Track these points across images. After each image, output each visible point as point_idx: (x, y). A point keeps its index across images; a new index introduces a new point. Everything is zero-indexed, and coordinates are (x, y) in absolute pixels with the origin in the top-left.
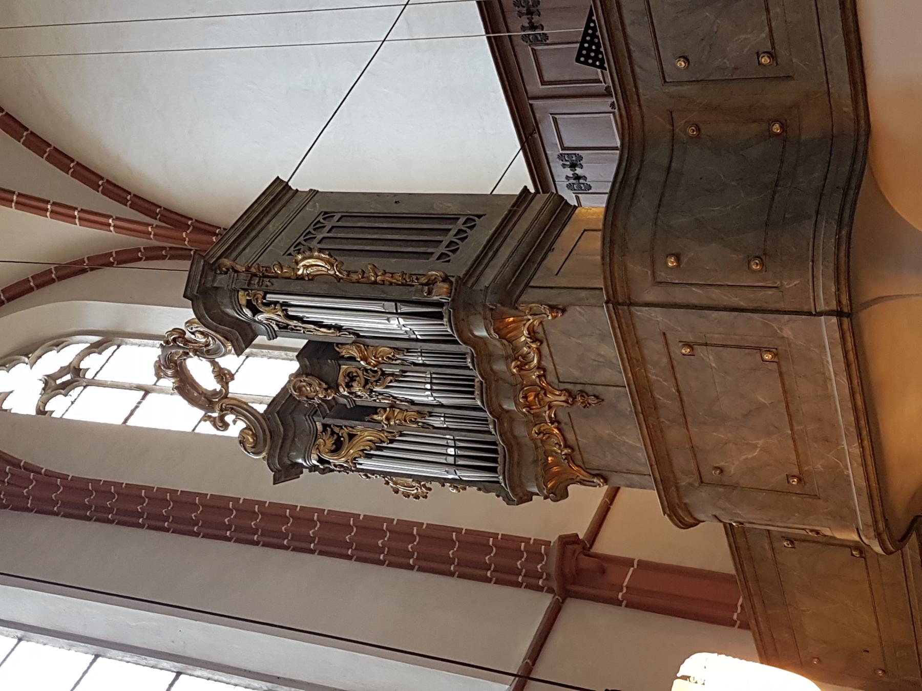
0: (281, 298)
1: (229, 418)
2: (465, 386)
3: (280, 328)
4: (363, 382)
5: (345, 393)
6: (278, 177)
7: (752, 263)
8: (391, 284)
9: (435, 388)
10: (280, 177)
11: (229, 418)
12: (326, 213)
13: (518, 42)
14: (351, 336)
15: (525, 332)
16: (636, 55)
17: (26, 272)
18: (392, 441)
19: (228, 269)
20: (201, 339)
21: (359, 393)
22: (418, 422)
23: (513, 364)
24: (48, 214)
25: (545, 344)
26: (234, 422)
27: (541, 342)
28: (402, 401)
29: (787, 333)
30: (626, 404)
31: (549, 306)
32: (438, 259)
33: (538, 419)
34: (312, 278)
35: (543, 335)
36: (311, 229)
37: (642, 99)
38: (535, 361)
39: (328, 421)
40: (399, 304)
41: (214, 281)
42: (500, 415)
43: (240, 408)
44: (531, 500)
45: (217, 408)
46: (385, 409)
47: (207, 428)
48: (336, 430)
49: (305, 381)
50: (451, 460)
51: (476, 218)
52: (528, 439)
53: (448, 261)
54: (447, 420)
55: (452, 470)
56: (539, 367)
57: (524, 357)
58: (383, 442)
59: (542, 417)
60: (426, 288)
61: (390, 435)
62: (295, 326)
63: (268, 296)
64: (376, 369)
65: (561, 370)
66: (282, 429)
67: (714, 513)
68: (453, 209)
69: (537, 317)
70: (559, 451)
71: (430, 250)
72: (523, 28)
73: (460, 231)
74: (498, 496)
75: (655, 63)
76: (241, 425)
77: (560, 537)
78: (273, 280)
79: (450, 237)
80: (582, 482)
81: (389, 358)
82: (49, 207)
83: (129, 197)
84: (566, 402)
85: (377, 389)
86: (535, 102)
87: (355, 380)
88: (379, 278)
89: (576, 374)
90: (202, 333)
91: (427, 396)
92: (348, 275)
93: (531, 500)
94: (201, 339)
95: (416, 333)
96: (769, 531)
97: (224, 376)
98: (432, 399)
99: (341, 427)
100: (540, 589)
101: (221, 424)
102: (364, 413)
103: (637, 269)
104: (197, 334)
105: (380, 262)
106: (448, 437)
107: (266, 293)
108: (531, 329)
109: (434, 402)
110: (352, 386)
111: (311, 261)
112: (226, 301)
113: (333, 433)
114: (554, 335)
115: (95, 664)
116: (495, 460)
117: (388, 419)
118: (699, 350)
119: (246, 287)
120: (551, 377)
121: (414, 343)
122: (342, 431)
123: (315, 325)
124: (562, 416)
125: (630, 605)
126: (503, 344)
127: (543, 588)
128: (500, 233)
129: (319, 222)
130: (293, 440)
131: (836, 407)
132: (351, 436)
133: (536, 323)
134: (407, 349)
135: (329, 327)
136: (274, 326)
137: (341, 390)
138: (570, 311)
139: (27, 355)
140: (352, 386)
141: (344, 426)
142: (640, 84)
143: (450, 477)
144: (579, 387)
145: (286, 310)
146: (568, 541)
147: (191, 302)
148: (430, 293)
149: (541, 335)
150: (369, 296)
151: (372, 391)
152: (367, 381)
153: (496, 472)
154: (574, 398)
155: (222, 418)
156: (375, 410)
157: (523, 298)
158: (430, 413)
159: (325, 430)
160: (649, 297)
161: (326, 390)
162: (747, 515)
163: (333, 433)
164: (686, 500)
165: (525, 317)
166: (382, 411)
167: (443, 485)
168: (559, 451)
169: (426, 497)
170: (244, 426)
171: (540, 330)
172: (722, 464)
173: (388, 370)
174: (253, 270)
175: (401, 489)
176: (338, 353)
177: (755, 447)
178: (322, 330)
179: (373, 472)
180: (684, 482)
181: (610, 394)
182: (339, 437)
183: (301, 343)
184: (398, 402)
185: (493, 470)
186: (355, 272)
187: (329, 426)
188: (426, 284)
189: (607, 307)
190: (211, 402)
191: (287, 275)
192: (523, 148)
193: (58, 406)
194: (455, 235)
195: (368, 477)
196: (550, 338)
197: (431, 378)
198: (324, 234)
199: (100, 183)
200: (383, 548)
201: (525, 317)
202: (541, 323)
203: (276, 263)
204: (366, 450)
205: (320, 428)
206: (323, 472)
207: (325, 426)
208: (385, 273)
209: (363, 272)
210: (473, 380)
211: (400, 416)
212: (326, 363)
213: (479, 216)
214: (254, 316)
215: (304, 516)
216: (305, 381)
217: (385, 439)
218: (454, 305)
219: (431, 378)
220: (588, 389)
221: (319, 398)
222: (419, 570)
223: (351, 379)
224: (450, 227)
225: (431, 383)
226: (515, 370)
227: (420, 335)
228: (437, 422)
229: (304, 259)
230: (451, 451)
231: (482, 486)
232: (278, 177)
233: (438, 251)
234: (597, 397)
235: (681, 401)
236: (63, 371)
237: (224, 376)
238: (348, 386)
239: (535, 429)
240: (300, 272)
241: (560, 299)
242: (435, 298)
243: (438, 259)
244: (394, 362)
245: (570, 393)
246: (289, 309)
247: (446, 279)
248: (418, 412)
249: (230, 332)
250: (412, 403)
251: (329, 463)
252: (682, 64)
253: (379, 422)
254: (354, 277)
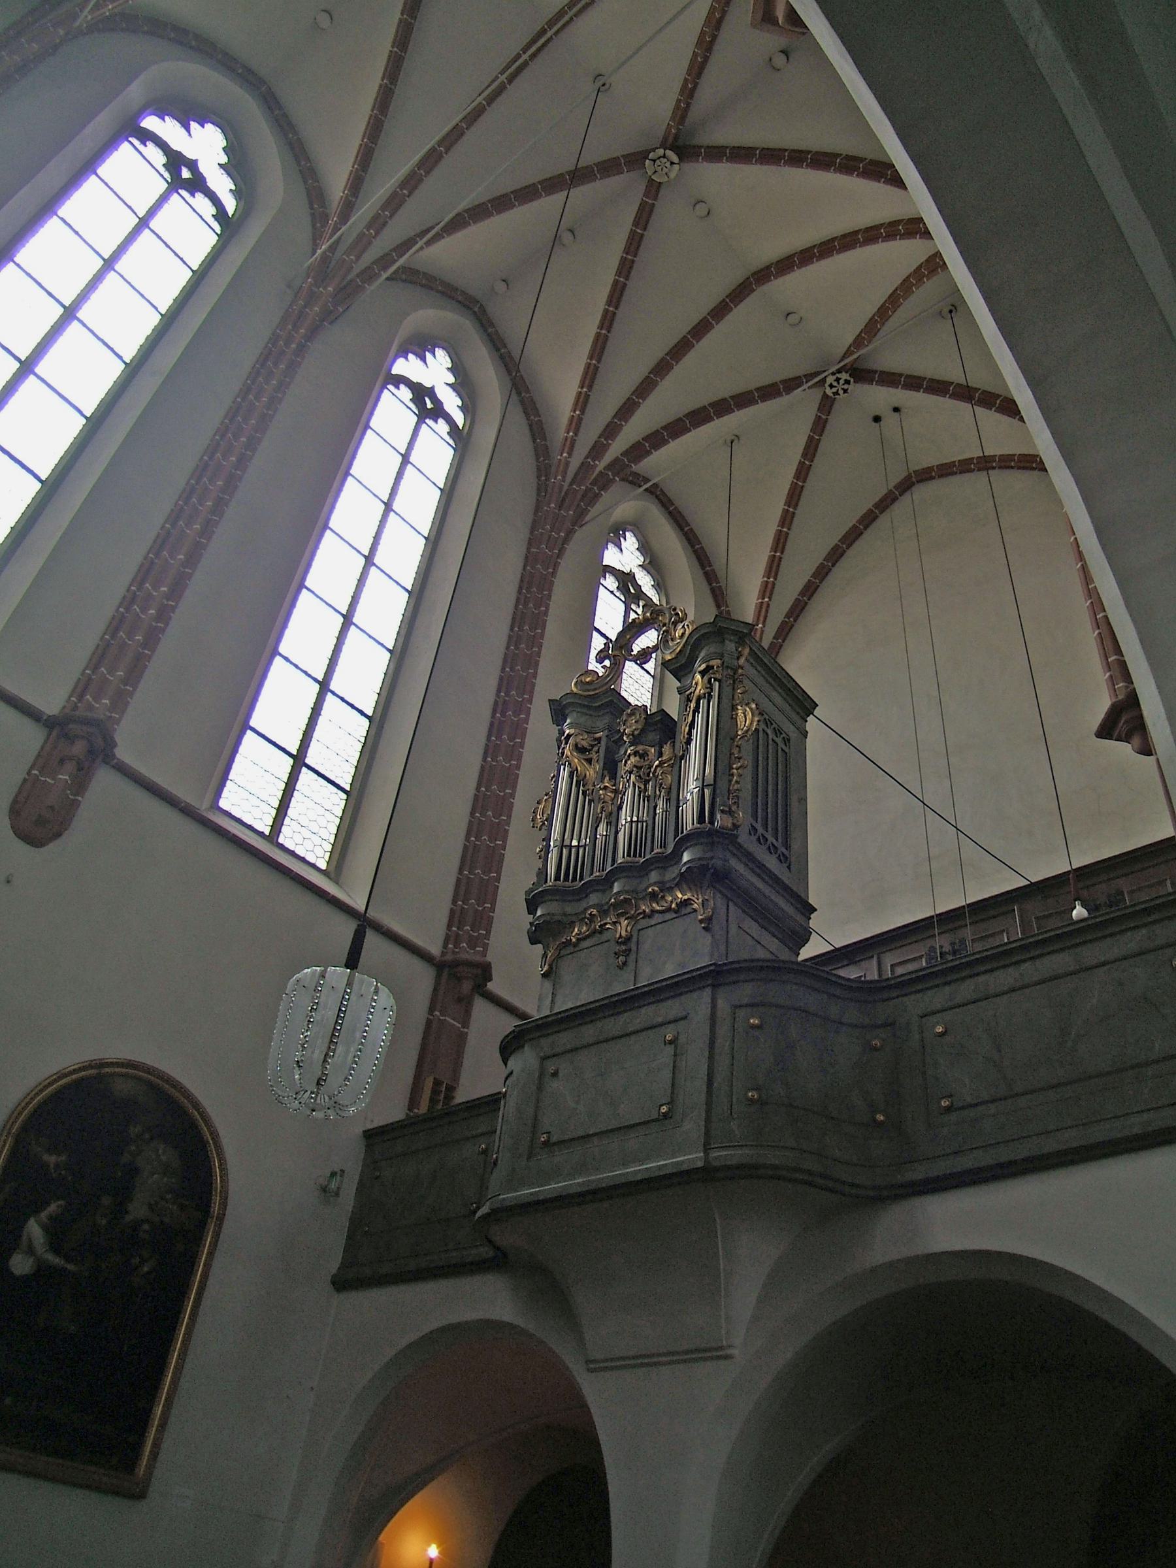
0: (715, 694)
1: (607, 663)
2: (634, 849)
3: (688, 696)
4: (639, 765)
5: (629, 751)
6: (817, 705)
7: (755, 1093)
8: (730, 781)
9: (634, 824)
10: (817, 708)
11: (607, 663)
12: (789, 740)
13: (929, 943)
14: (681, 753)
15: (686, 897)
16: (947, 989)
17: (718, 564)
18: (584, 793)
19: (740, 652)
20: (678, 633)
21: (629, 762)
22: (602, 813)
23: (656, 889)
24: (766, 579)
25: (675, 916)
26: (603, 667)
27: (676, 912)
28: (621, 798)
29: (687, 1126)
30: (618, 988)
31: (712, 916)
32: (752, 826)
33: (604, 913)
34: (734, 719)
35: (683, 913)
36: (775, 725)
37: (905, 999)
38: (658, 908)
39: (603, 742)
40: (712, 787)
41: (731, 641)
42: (606, 882)
43: (616, 671)
44: (529, 914)
45: (616, 653)
46: (614, 785)
47: (598, 643)
48: (596, 749)
49: (640, 717)
50: (567, 842)
51: (787, 864)
52: (585, 906)
53: (750, 834)
54: (604, 837)
55: (558, 843)
56: (653, 911)
57: (663, 897)
58: (584, 786)
59: (607, 918)
60: (727, 809)
61: (591, 791)
62: (690, 707)
63: (717, 683)
64: (651, 775)
65: (650, 931)
66: (597, 704)
67: (514, 1073)
68: (795, 846)
69: (701, 907)
70: (574, 934)
71: (759, 819)
72: (941, 947)
73: (776, 848)
74: (533, 884)
75: (939, 1006)
76: (601, 672)
77: (490, 963)
78: (731, 687)
79: (771, 839)
80: (545, 955)
81: (661, 784)
82: (778, 554)
83: (791, 619)
84: (621, 936)
85: (633, 777)
86: (874, 961)
87: (640, 758)
88: (735, 771)
89: (646, 946)
90: (683, 634)
91: (626, 819)
92: (737, 746)
93: (529, 914)
94: (678, 633)
95: (685, 806)
96: (496, 1132)
97: (643, 657)
98: (624, 823)
99: (598, 752)
100: (445, 946)
101: (602, 656)
102: (611, 767)
103: (746, 992)
104: (682, 631)
105: (748, 773)
106: (588, 840)
107: (719, 681)
108: (688, 902)
109: (620, 826)
110: (635, 756)
111: (749, 716)
112: (712, 650)
113: (593, 746)
114: (680, 924)
115: (385, 650)
116: (566, 878)
117: (605, 788)
118: (670, 1049)
119: (725, 664)
120: (644, 923)
121: (675, 805)
122: (594, 753)
123: (691, 721)
124: (606, 936)
125: (429, 1023)
126: (674, 879)
127: (432, 1015)
128: (776, 881)
129: (781, 733)
130: (587, 714)
131: (616, 1171)
132: (589, 761)
133: (695, 906)
134: (669, 799)
135: (690, 733)
136: (690, 691)
137: (632, 748)
138: (708, 937)
139: (650, 563)
140: (635, 756)
141: (598, 757)
142: (919, 996)
143: (552, 843)
144: (634, 948)
145: (705, 697)
146: (485, 972)
147: (712, 621)
148: (722, 811)
149: (684, 911)
150: (719, 762)
151: (631, 773)
152: (639, 768)
153: (555, 880)
154: (624, 943)
155: (608, 657)
156: (613, 777)
157: (718, 895)
158: (611, 823)
159: (595, 739)
160: (721, 1003)
161: (633, 735)
162: (509, 1108)
163: (593, 746)
164: (526, 1048)
165: (700, 896)
166: (612, 783)
167: (543, 840)
168: (574, 934)
169: (533, 827)
170: (600, 674)
171: (689, 910)
172: (561, 1074)
173: (650, 786)
174: (740, 671)
175: (541, 807)
176: (666, 744)
177: (577, 1103)
178: (687, 728)
179: (557, 782)
180: (545, 1042)
181: (628, 974)
182: (589, 751)
183: (673, 711)
184: (620, 796)
185: (557, 878)
186: (740, 752)
187: (599, 743)
188: (730, 809)
189: (711, 965)
190: (621, 648)
191: (736, 697)
192: (836, 950)
193: (610, 582)
194: (773, 845)
195: (552, 778)
196: (680, 920)
197: (643, 822)
198: (771, 735)
199: (791, 619)
200: (480, 841)
201: (700, 896)
202: (695, 911)
203: (747, 688)
204: (577, 772)
205: (598, 735)
206: (559, 741)
207: (599, 740)
208: (740, 775)
209: (739, 758)
210: (640, 856)
211: (607, 798)
212: (656, 735)
213: (789, 867)
214: (700, 672)
215: (519, 731)
216: (640, 717)
217: (587, 787)
218: (711, 833)
219: (643, 822)
220: (632, 957)
221: (625, 730)
222: (470, 821)
223: (643, 755)
224: (780, 840)
225: (637, 822)
226: (650, 890)
227: (682, 809)
228: (602, 830)
229: (751, 709)
230: (575, 843)
231: (542, 873)
232: (817, 705)
233: (759, 826)
234: (625, 964)
235: (621, 1037)
236: (638, 587)
237: (643, 657)
238: (635, 753)
239: (595, 912)
240: (739, 707)
241: (716, 926)
242: (718, 817)
243: (752, 826)
244: (657, 789)
245: (628, 939)
246: (706, 701)
247: (735, 826)
248: (611, 814)
249: (685, 655)
250: (620, 808)
251: (566, 743)
252: (940, 1029)
253: (602, 781)
254: (735, 751)
